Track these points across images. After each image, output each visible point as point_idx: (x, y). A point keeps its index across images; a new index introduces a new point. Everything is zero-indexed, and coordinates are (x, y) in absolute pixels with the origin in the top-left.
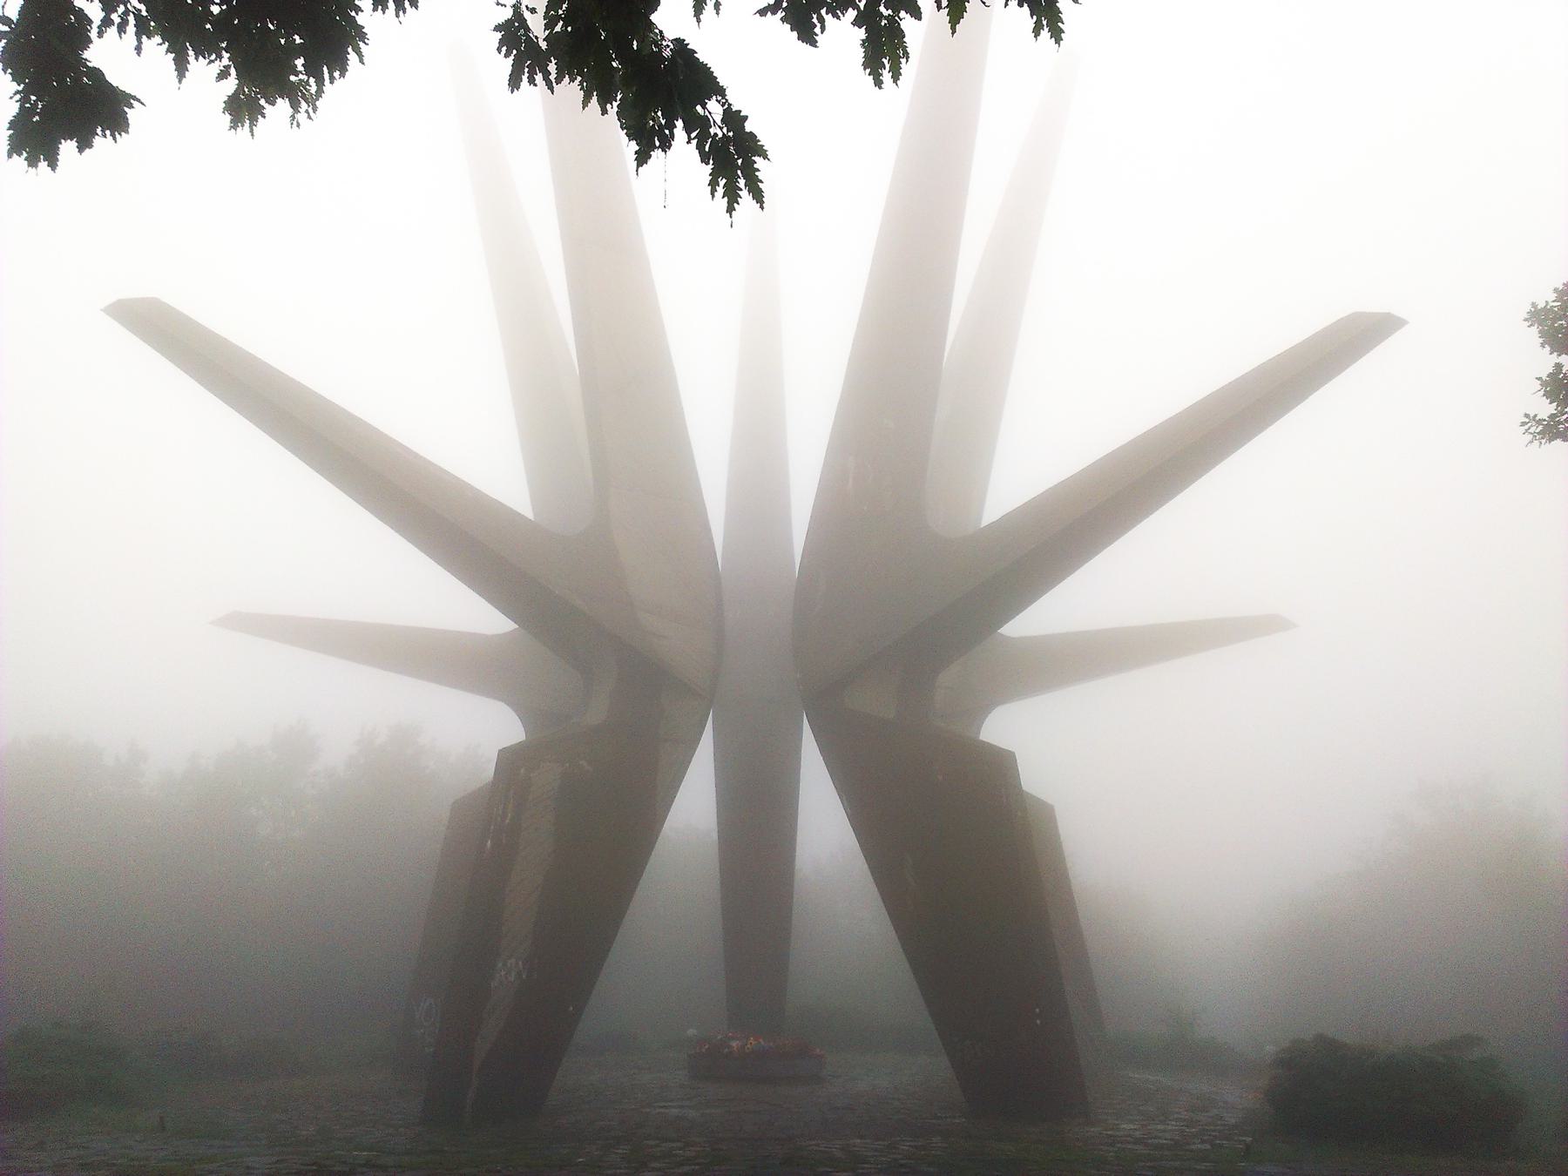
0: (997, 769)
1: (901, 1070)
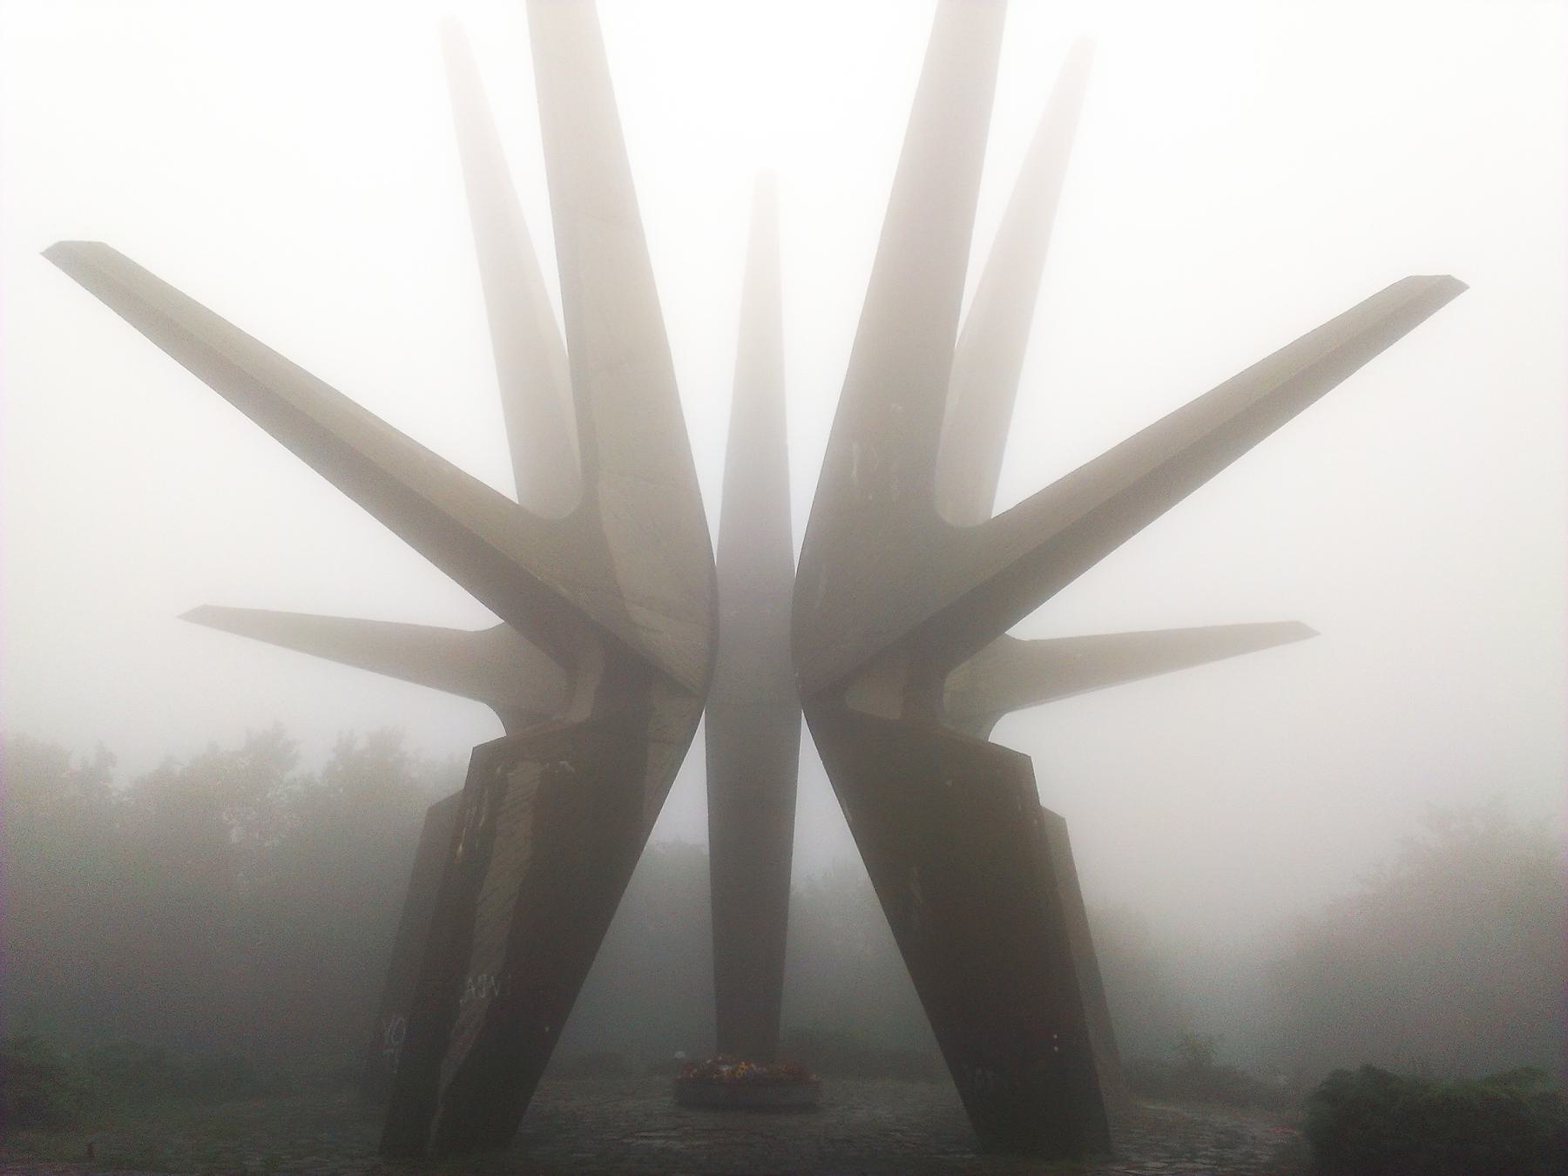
0: (1011, 775)
1: (918, 1098)
